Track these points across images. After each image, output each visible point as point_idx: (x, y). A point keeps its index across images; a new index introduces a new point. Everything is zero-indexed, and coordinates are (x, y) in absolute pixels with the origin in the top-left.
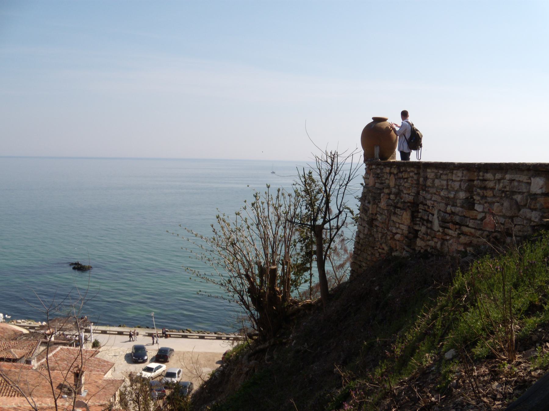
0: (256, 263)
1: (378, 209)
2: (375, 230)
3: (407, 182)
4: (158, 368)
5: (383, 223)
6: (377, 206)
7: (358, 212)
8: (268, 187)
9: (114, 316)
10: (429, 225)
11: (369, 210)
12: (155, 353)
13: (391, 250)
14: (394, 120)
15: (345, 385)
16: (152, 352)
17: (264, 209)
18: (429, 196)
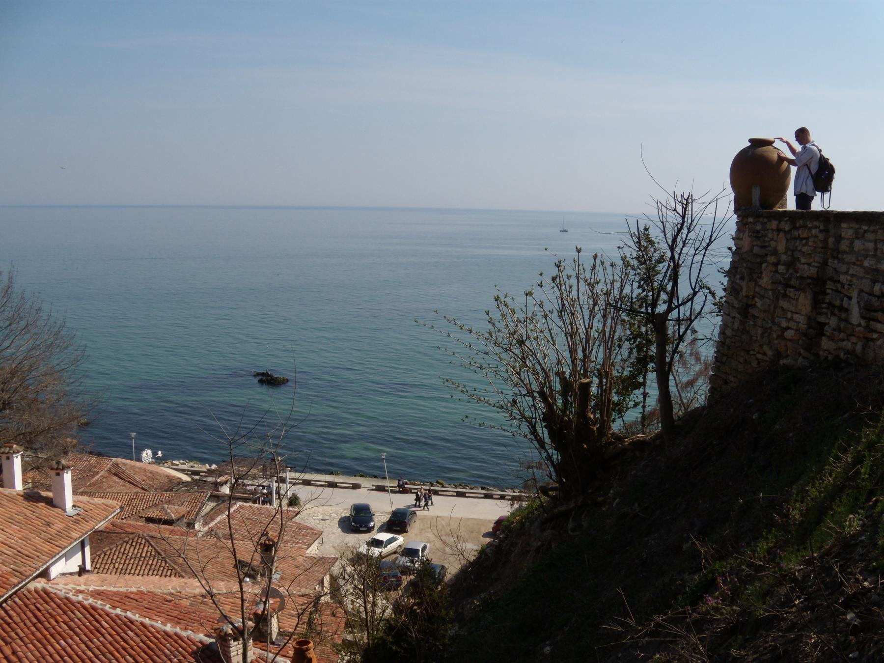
0: (557, 374)
1: (757, 289)
2: (751, 323)
3: (806, 244)
4: (390, 541)
5: (765, 311)
6: (756, 284)
7: (723, 294)
8: (579, 251)
9: (324, 458)
10: (843, 315)
11: (742, 289)
12: (385, 518)
13: (779, 355)
14: (784, 145)
15: (705, 568)
16: (381, 517)
17: (570, 287)
18: (844, 268)
